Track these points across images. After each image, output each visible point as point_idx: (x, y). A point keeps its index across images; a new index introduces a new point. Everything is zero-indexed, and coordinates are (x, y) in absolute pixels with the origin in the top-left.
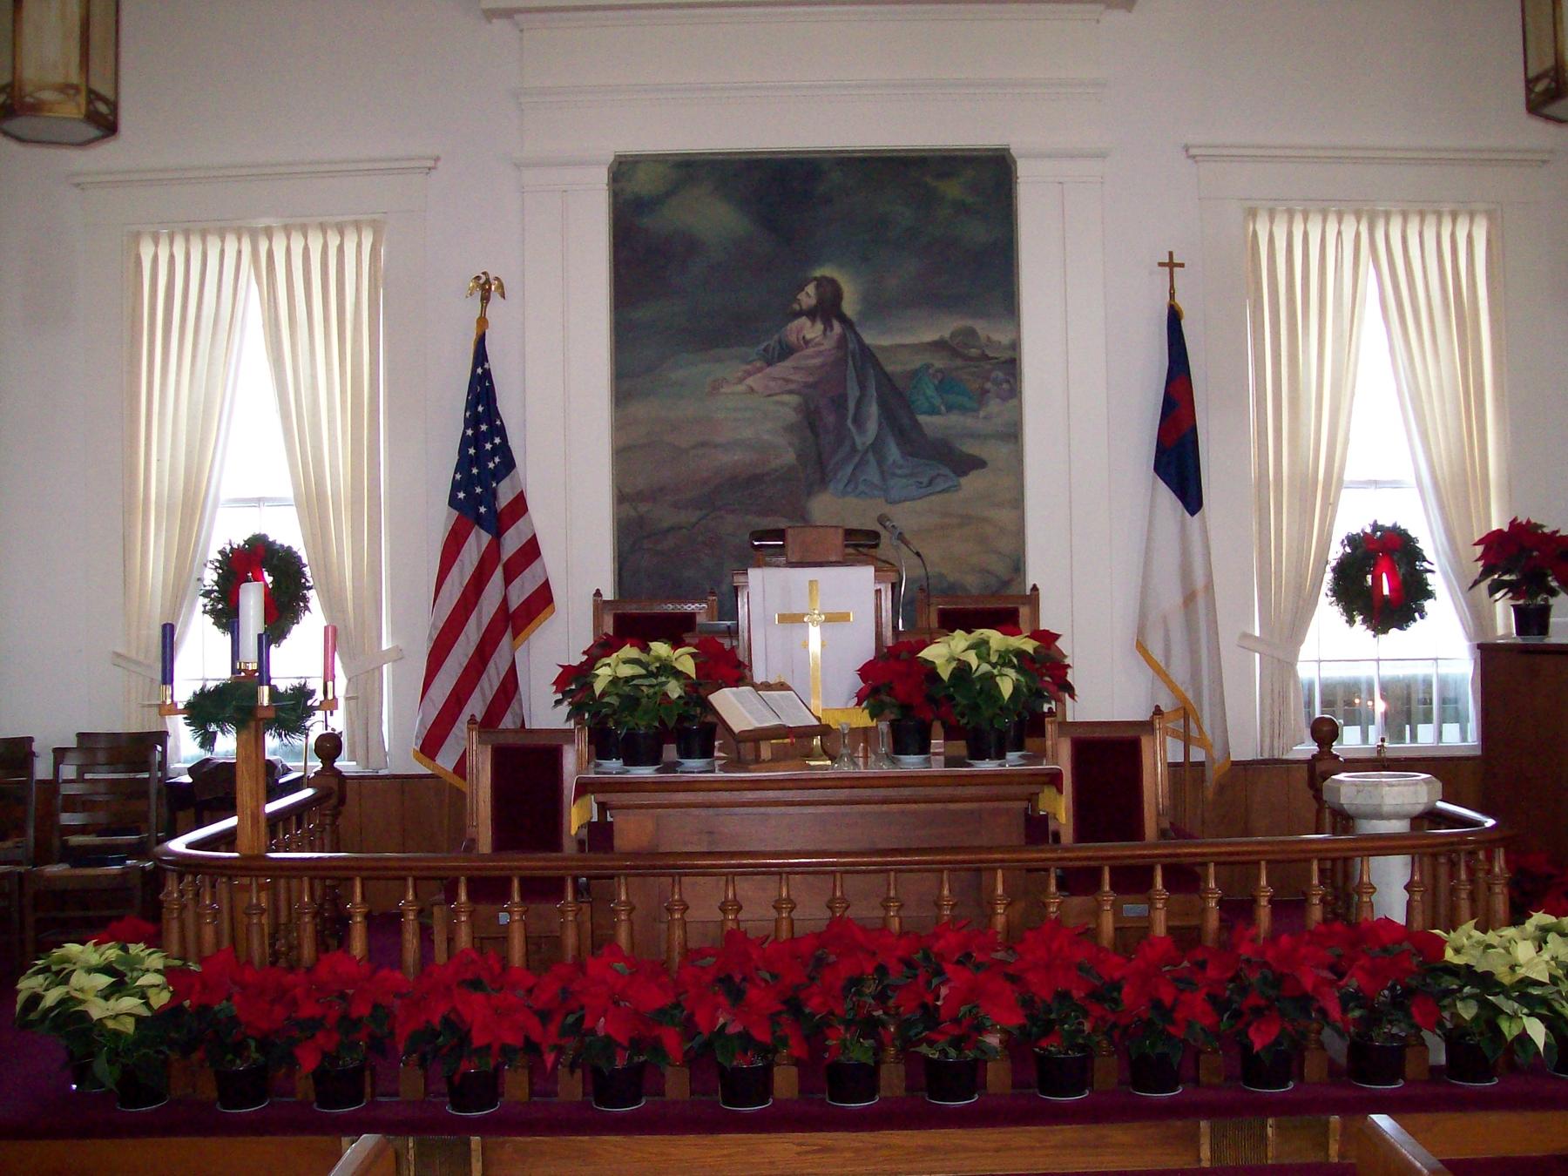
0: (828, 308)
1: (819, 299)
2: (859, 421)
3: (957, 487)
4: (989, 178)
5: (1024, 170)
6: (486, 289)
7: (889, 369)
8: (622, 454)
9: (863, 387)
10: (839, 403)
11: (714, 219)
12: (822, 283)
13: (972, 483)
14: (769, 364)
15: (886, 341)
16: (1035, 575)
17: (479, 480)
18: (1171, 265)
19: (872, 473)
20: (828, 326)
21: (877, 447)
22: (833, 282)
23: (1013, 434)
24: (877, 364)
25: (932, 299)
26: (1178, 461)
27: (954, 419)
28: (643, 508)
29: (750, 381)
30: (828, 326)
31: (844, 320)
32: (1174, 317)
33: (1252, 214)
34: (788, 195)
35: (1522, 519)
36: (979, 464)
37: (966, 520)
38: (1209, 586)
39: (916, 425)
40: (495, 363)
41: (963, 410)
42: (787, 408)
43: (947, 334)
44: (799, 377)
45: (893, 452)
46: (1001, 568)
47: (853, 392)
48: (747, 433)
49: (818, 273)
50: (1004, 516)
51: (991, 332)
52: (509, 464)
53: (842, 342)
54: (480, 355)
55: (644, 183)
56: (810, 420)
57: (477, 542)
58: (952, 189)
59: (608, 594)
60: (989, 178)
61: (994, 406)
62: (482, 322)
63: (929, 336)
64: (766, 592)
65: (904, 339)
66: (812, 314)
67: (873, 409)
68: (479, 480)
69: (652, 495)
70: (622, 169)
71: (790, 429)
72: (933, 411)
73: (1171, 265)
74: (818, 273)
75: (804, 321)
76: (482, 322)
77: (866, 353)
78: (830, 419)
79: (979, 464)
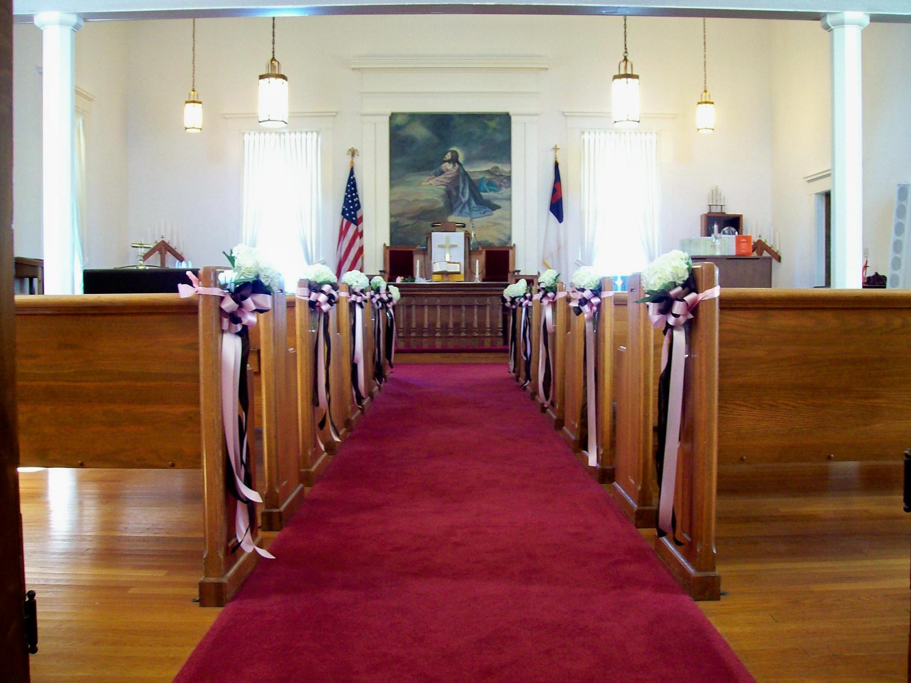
0: (454, 160)
1: (449, 152)
2: (463, 194)
3: (491, 214)
4: (506, 119)
5: (513, 119)
6: (353, 153)
7: (472, 178)
8: (392, 202)
9: (464, 184)
10: (457, 188)
11: (420, 132)
12: (453, 152)
13: (497, 213)
14: (436, 176)
15: (472, 170)
16: (514, 241)
17: (352, 210)
18: (556, 149)
19: (467, 210)
20: (454, 165)
21: (468, 202)
22: (456, 152)
23: (509, 199)
24: (469, 178)
25: (485, 158)
26: (556, 208)
27: (492, 194)
28: (398, 219)
29: (431, 182)
30: (454, 165)
31: (459, 164)
32: (557, 165)
33: (583, 133)
34: (443, 125)
35: (881, 273)
36: (499, 207)
37: (495, 224)
38: (566, 243)
39: (481, 196)
40: (357, 175)
41: (495, 191)
42: (441, 190)
43: (490, 168)
44: (446, 181)
45: (473, 203)
46: (504, 238)
47: (461, 185)
48: (429, 197)
49: (452, 149)
50: (507, 223)
51: (503, 168)
52: (359, 207)
53: (458, 170)
54: (352, 173)
55: (399, 120)
56: (448, 194)
57: (353, 228)
58: (492, 124)
59: (388, 244)
60: (506, 119)
61: (504, 190)
62: (352, 162)
63: (486, 169)
64: (438, 238)
65: (478, 169)
66: (449, 161)
67: (467, 191)
68: (352, 210)
69: (401, 215)
70: (393, 116)
71: (443, 196)
72: (485, 191)
73: (556, 149)
74: (452, 149)
75: (447, 164)
76: (352, 162)
77: (466, 174)
78: (454, 193)
79: (499, 207)
